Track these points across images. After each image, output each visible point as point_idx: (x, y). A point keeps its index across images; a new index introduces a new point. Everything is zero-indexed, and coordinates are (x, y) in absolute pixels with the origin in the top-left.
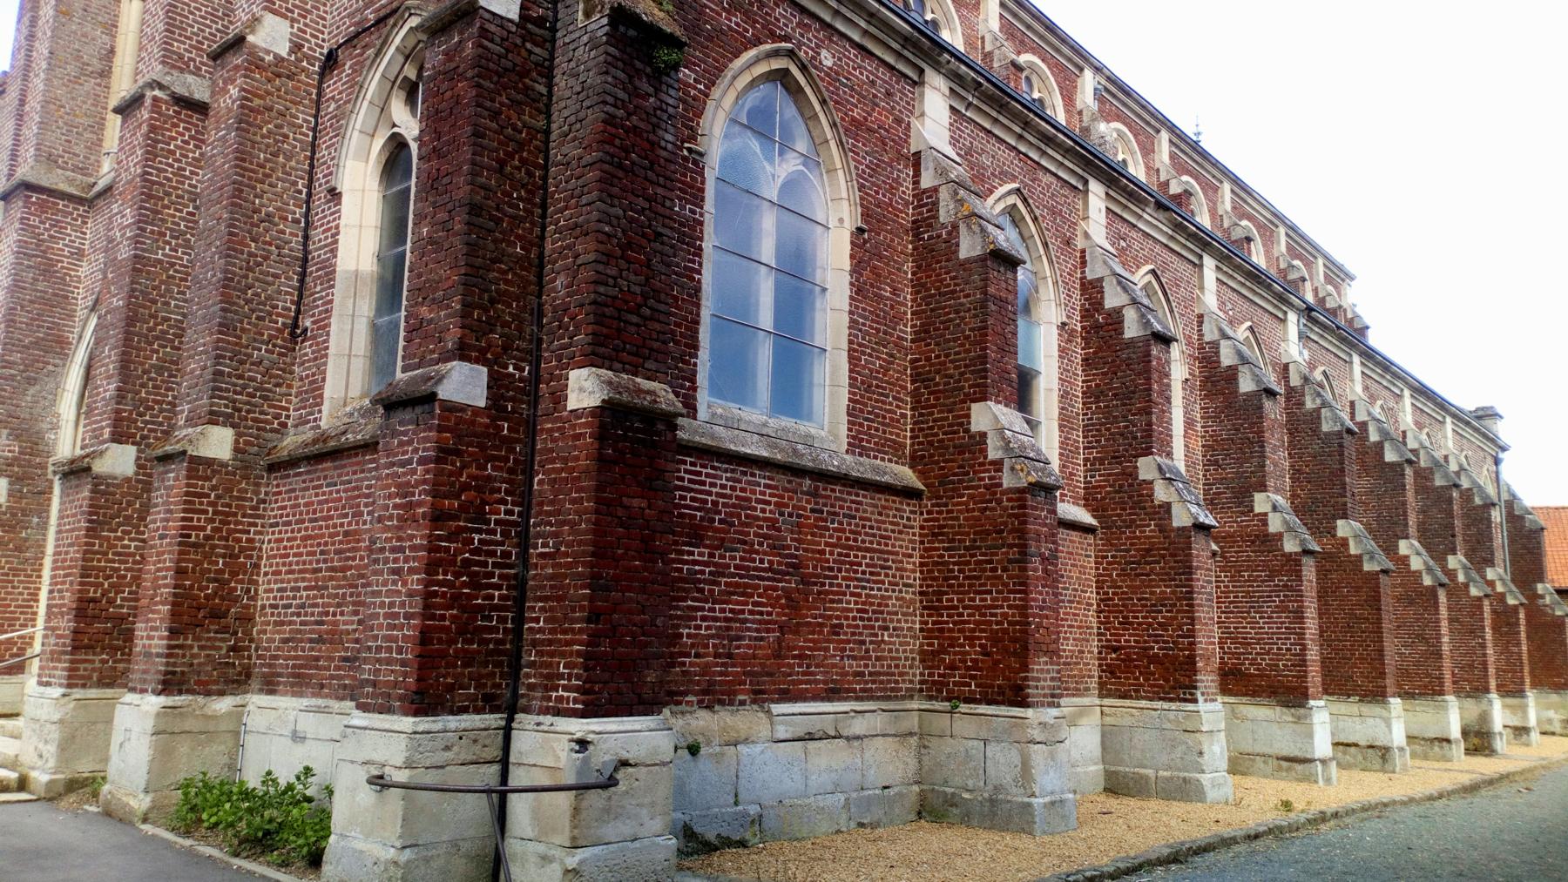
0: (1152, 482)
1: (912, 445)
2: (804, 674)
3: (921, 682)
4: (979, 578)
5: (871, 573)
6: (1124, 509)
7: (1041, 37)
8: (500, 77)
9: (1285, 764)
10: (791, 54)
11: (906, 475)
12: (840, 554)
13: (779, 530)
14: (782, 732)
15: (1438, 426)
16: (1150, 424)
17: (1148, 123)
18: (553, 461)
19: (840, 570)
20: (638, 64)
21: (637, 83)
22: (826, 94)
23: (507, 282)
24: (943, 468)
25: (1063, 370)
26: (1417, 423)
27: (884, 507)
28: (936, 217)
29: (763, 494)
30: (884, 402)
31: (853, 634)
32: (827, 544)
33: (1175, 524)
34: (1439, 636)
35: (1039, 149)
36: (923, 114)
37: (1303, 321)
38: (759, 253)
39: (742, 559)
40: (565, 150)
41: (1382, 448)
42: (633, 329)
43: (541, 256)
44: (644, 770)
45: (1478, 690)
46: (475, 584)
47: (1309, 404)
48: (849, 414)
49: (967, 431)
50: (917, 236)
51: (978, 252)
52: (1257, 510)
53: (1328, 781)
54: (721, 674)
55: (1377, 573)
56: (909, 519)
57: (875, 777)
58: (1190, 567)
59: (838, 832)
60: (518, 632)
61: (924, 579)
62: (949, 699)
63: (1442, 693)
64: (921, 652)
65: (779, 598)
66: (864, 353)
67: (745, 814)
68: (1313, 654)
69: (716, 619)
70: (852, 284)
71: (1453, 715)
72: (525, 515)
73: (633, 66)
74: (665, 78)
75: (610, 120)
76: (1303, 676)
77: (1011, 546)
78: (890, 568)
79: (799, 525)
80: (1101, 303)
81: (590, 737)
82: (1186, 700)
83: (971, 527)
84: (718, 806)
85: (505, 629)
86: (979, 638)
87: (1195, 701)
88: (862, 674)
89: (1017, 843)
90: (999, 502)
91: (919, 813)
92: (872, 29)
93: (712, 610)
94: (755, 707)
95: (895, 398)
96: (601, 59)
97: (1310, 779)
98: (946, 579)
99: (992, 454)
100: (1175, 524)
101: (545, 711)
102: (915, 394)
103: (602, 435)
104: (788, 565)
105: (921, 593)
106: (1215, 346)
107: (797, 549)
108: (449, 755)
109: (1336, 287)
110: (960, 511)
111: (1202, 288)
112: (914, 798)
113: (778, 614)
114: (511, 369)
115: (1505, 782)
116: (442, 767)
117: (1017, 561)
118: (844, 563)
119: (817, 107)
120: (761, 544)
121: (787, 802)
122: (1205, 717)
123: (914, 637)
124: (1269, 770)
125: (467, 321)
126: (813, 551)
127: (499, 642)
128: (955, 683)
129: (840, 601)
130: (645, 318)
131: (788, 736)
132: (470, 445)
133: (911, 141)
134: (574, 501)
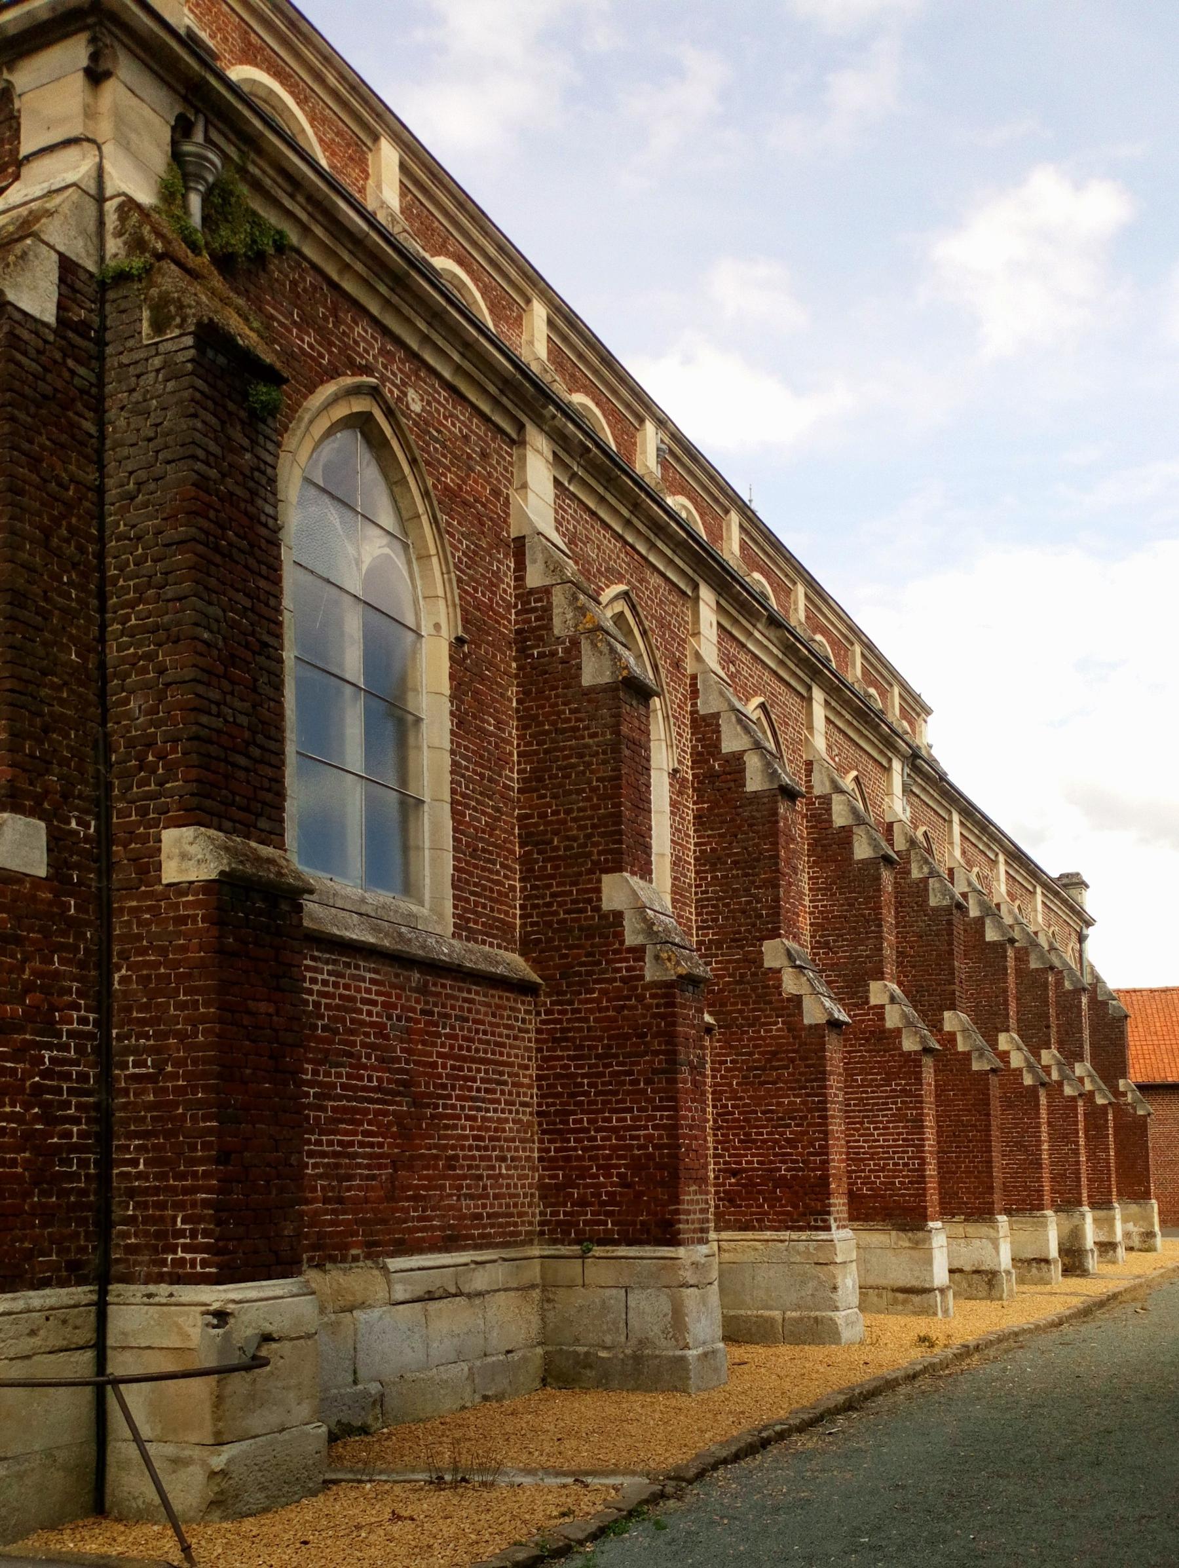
0: (779, 971)
1: (523, 926)
2: (421, 1219)
3: (541, 1224)
4: (615, 1093)
5: (487, 1091)
6: (746, 1004)
7: (596, 372)
8: (39, 407)
9: (900, 1296)
10: (374, 392)
11: (513, 963)
12: (453, 1068)
13: (386, 1037)
14: (400, 1293)
15: (1028, 897)
16: (777, 900)
17: (716, 500)
18: (143, 952)
19: (453, 1088)
20: (231, 406)
21: (230, 431)
22: (417, 452)
23: (62, 702)
24: (565, 956)
25: (676, 830)
26: (1009, 893)
27: (498, 1007)
28: (549, 628)
29: (368, 991)
30: (491, 871)
31: (470, 1167)
32: (440, 1055)
33: (806, 1022)
34: (1039, 1143)
35: (648, 540)
36: (524, 486)
37: (907, 770)
38: (341, 665)
39: (349, 1076)
40: (132, 515)
41: (983, 924)
42: (241, 775)
43: (102, 666)
44: (288, 1345)
45: (1068, 1204)
46: (48, 1118)
47: (916, 874)
48: (454, 887)
49: (597, 909)
50: (523, 652)
51: (606, 678)
52: (873, 1001)
53: (946, 1312)
54: (332, 1223)
55: (987, 1073)
56: (524, 1021)
57: (497, 1341)
58: (824, 1072)
59: (464, 1408)
60: (104, 1178)
61: (543, 1096)
62: (578, 1242)
63: (1040, 1208)
64: (542, 1187)
65: (390, 1124)
66: (467, 806)
67: (366, 1394)
68: (931, 1170)
69: (324, 1154)
70: (452, 714)
71: (1051, 1233)
72: (104, 1024)
73: (224, 407)
74: (261, 426)
75: (202, 483)
76: (922, 1194)
77: (656, 1053)
78: (505, 1083)
79: (408, 1031)
80: (717, 745)
81: (231, 1307)
82: (817, 1229)
83: (603, 1030)
84: (338, 1387)
85: (87, 1176)
86: (618, 1167)
87: (828, 1229)
88: (478, 1217)
89: (674, 1403)
90: (640, 998)
91: (543, 1380)
92: (466, 365)
93: (319, 1143)
94: (369, 1263)
95: (503, 866)
96: (186, 394)
97: (928, 1311)
98: (573, 1095)
99: (631, 939)
100: (806, 1022)
101: (160, 1279)
102: (525, 860)
103: (220, 919)
104: (397, 1082)
105: (539, 1114)
106: (826, 800)
107: (407, 1062)
108: (35, 1341)
109: (911, 724)
110: (591, 1011)
111: (810, 728)
112: (538, 1362)
113: (390, 1146)
114: (74, 825)
115: (1113, 1304)
116: (28, 1357)
117: (664, 1071)
118: (458, 1078)
119: (406, 469)
120: (368, 1057)
121: (408, 1375)
122: (839, 1245)
123: (533, 1169)
124: (883, 1303)
125: (19, 757)
126: (426, 1064)
127: (83, 1193)
128: (586, 1223)
129: (455, 1127)
130: (255, 761)
131: (408, 1296)
132: (31, 929)
133: (511, 521)
134: (181, 1006)
